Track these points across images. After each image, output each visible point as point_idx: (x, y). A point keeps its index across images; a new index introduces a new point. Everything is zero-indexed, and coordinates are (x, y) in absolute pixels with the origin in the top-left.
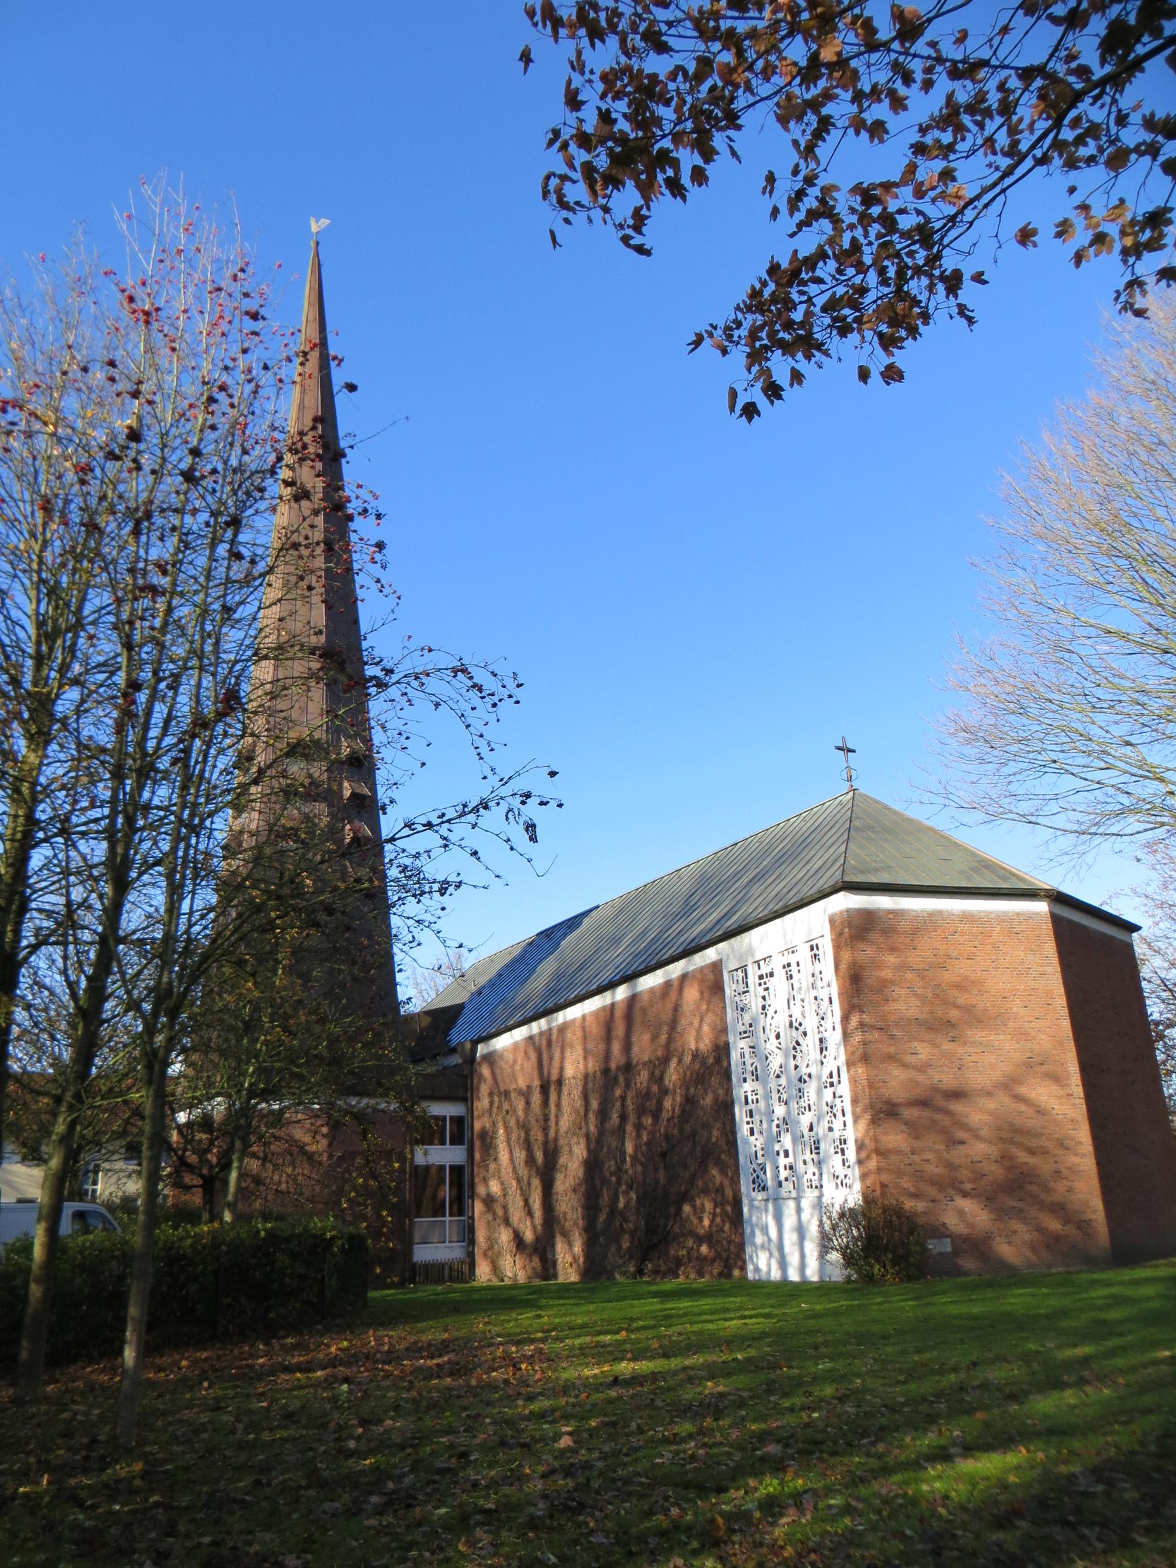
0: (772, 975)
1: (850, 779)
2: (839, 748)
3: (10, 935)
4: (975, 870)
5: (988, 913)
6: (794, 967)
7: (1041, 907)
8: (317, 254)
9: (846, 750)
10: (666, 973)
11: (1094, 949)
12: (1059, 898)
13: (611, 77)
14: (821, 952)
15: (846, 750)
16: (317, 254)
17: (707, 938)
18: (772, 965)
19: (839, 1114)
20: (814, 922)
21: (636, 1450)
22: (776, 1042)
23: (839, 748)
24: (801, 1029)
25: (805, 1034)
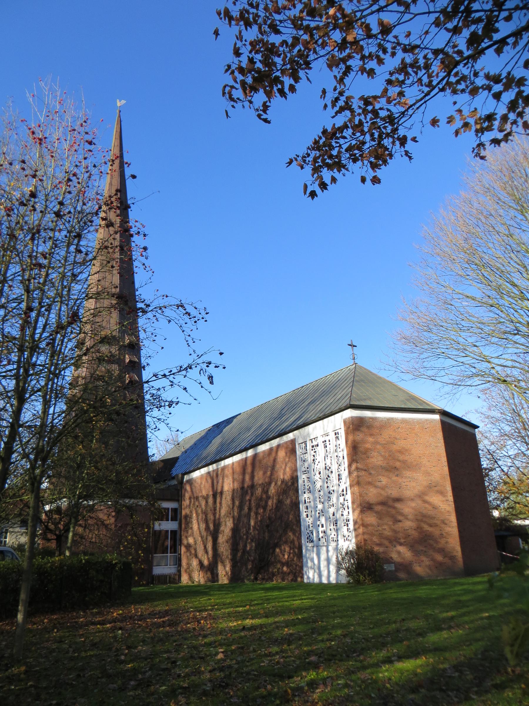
0: (317, 445)
1: (354, 359)
4: (407, 400)
5: (413, 419)
6: (327, 443)
7: (437, 417)
9: (353, 346)
12: (444, 413)
14: (339, 436)
15: (353, 346)
19: (346, 508)
20: (337, 422)
22: (319, 476)
24: (330, 470)
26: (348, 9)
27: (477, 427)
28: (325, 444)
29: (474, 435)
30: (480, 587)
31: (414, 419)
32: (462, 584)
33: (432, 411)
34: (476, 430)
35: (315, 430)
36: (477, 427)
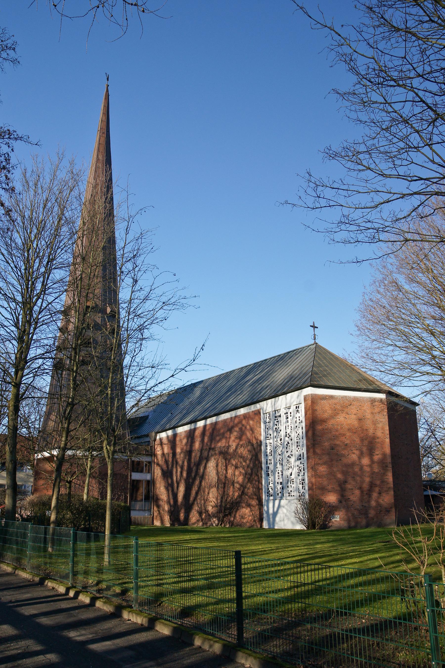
0: (280, 416)
1: (315, 339)
2: (311, 326)
3: (306, 588)
4: (360, 380)
5: (363, 398)
6: (289, 414)
7: (383, 396)
8: (107, 91)
9: (314, 327)
10: (250, 409)
11: (402, 415)
12: (390, 393)
13: (100, 556)
14: (300, 409)
15: (314, 327)
16: (107, 91)
17: (261, 398)
18: (280, 413)
19: (302, 470)
20: (294, 398)
21: (208, 561)
22: (280, 442)
23: (311, 326)
24: (290, 438)
25: (291, 440)
26: (2, 374)
27: (418, 405)
28: (285, 417)
29: (415, 411)
30: (249, 560)
31: (364, 398)
32: (340, 535)
33: (378, 391)
34: (417, 407)
35: (282, 402)
36: (418, 405)
